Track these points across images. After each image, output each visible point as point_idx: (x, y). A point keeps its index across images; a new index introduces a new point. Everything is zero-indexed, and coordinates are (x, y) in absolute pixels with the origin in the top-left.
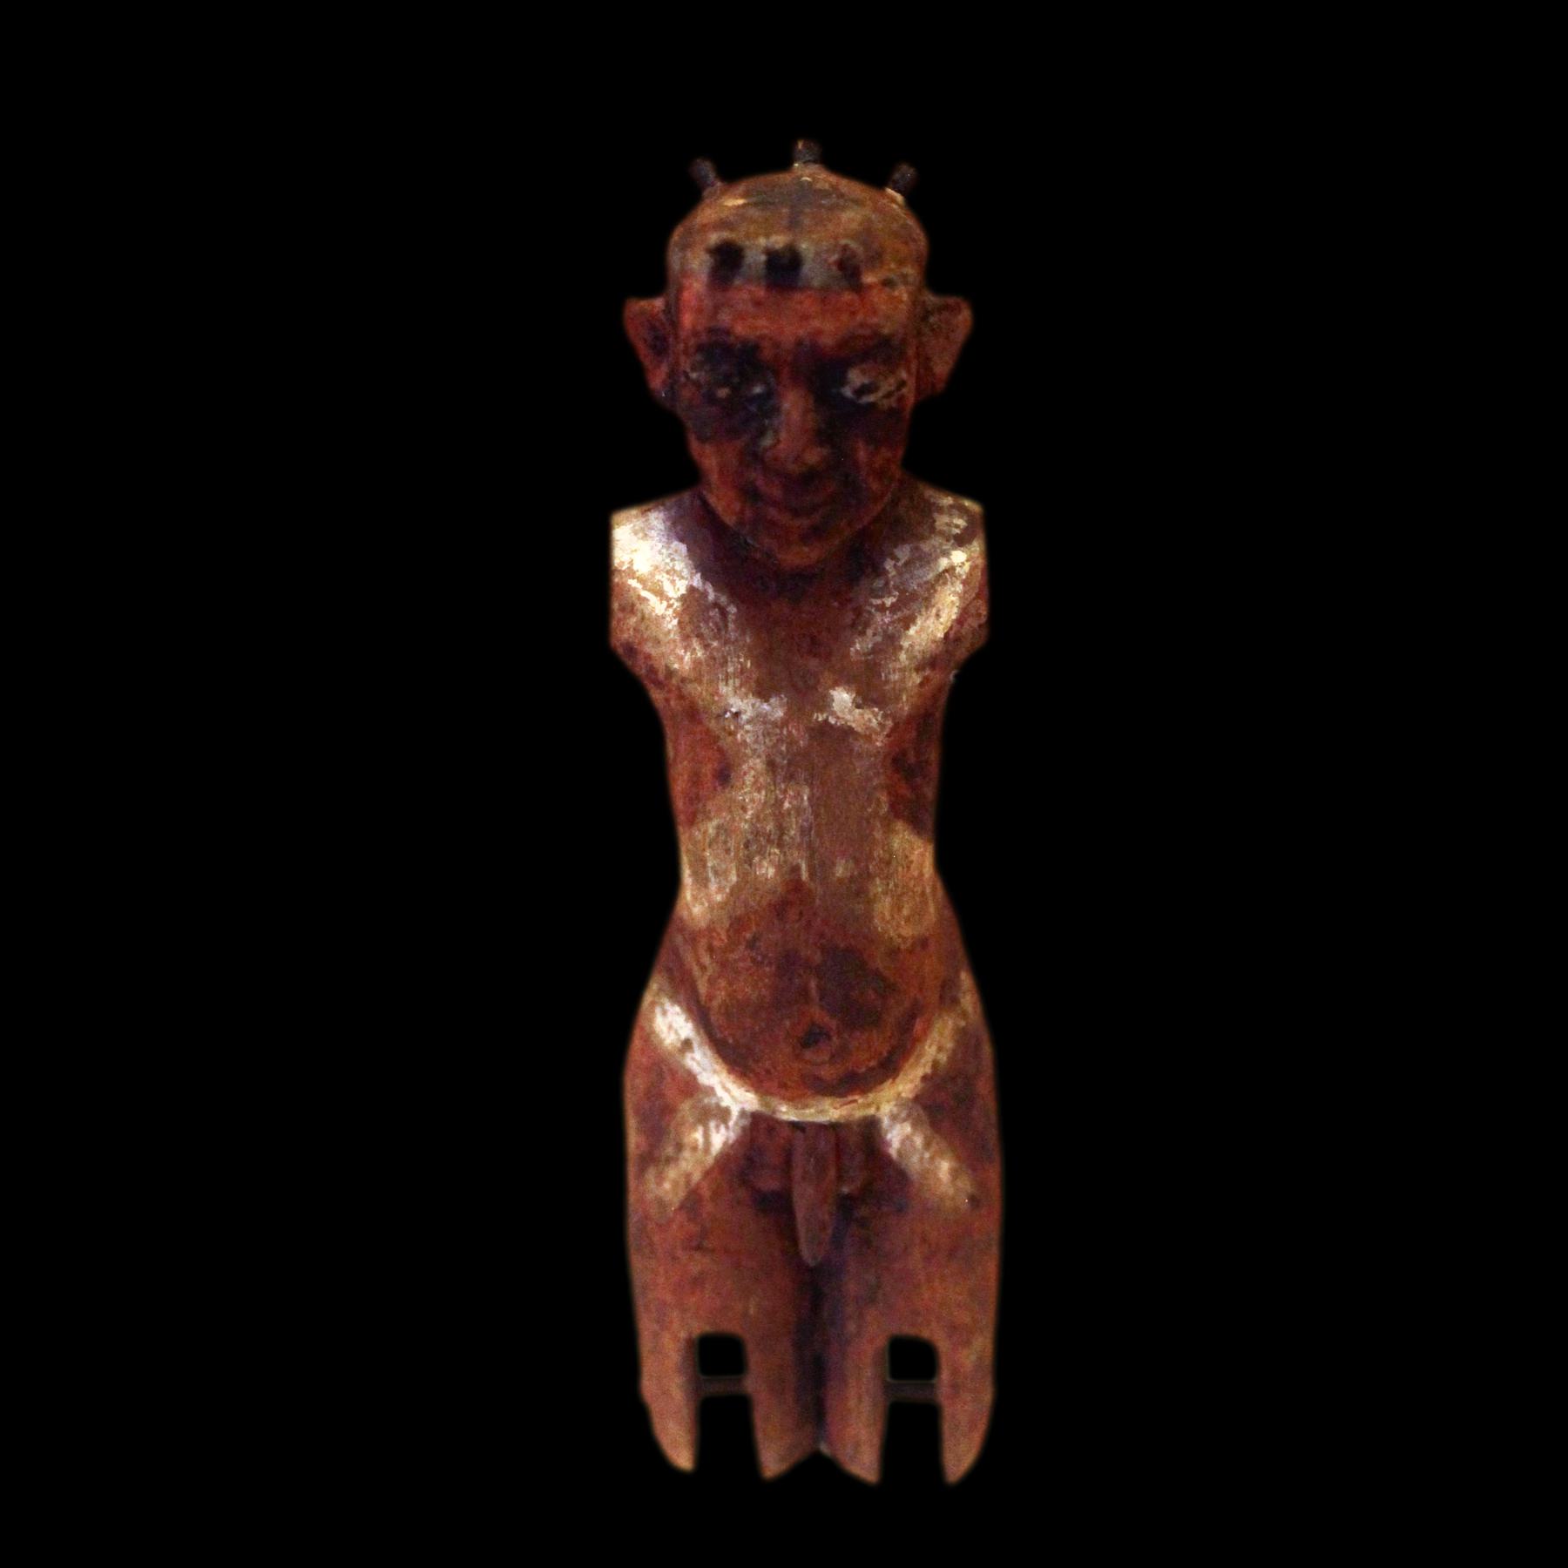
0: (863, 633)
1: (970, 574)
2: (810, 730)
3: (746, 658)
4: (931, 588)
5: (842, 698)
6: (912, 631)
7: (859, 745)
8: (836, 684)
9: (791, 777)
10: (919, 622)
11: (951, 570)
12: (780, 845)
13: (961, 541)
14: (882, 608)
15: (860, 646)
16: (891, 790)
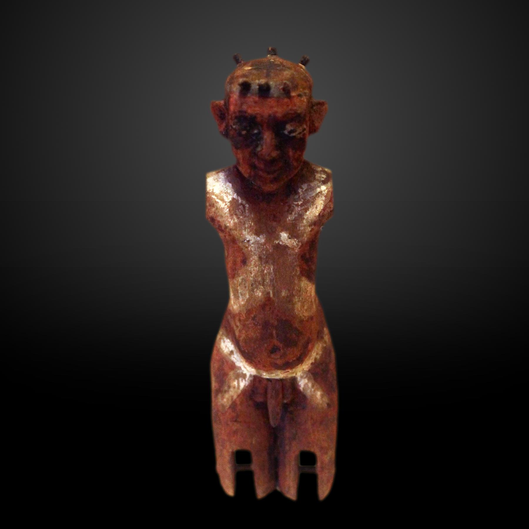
0: (291, 214)
1: (327, 194)
2: (273, 246)
3: (252, 222)
4: (314, 198)
5: (284, 235)
6: (308, 213)
7: (290, 251)
8: (282, 231)
9: (267, 262)
10: (310, 210)
11: (321, 192)
12: (263, 285)
14: (297, 205)
15: (290, 218)
16: (301, 267)
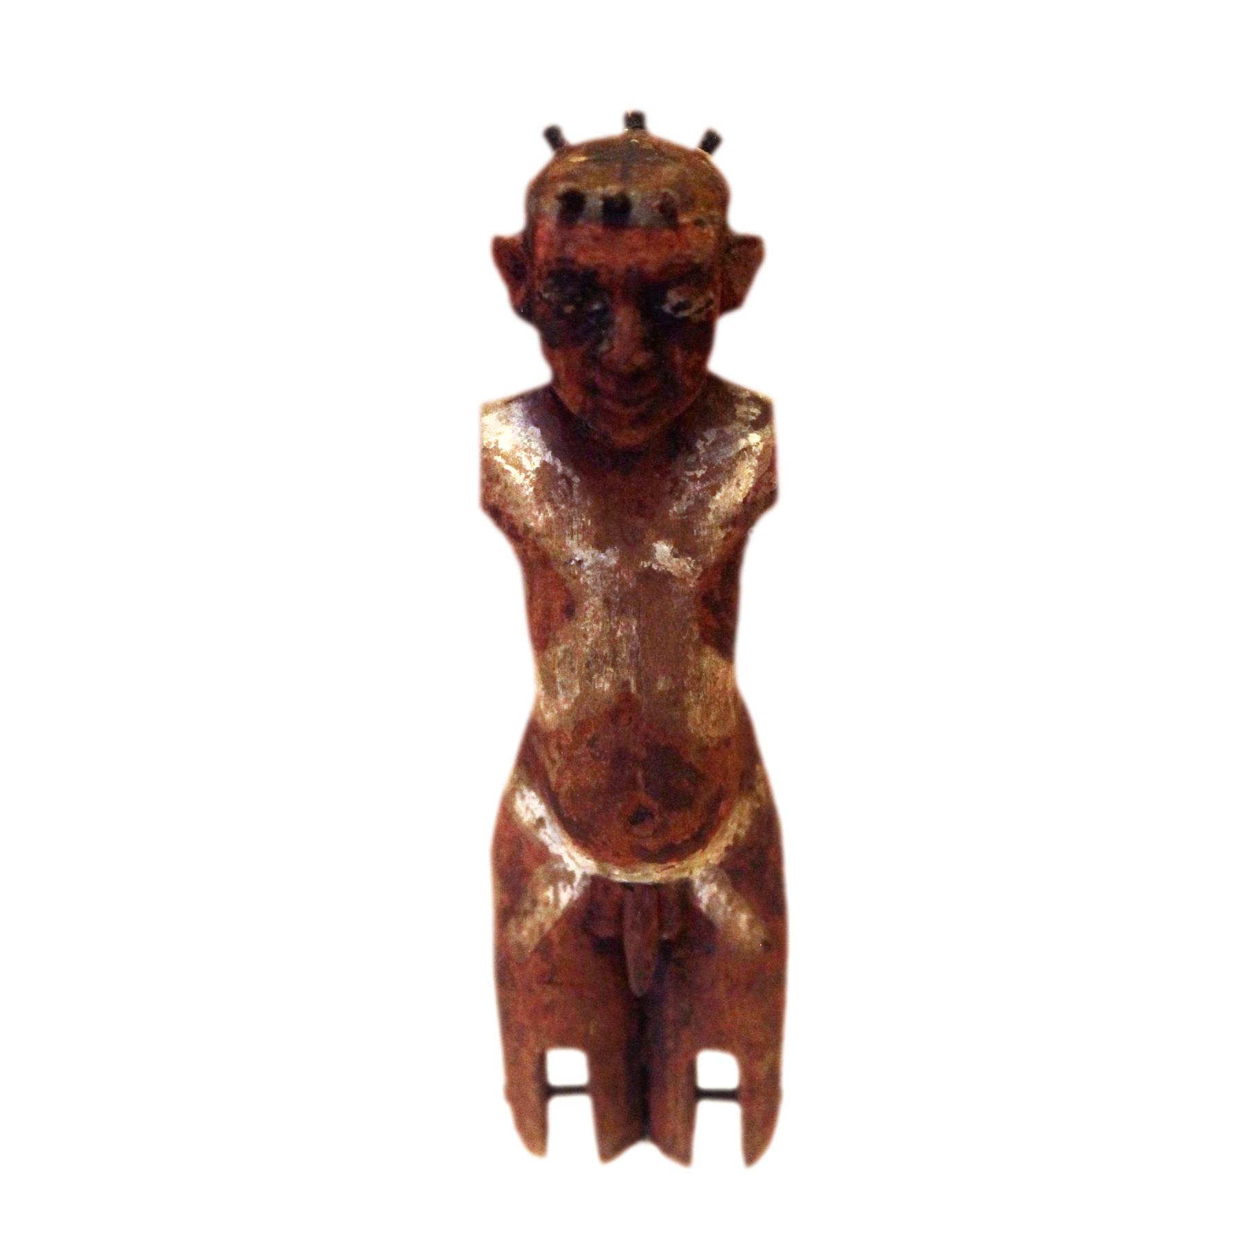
0: (679, 498)
2: (638, 574)
3: (587, 518)
4: (733, 463)
5: (663, 549)
6: (718, 497)
7: (676, 587)
8: (658, 538)
9: (622, 612)
10: (723, 489)
11: (748, 448)
12: (614, 665)
14: (694, 479)
15: (677, 508)
16: (701, 622)
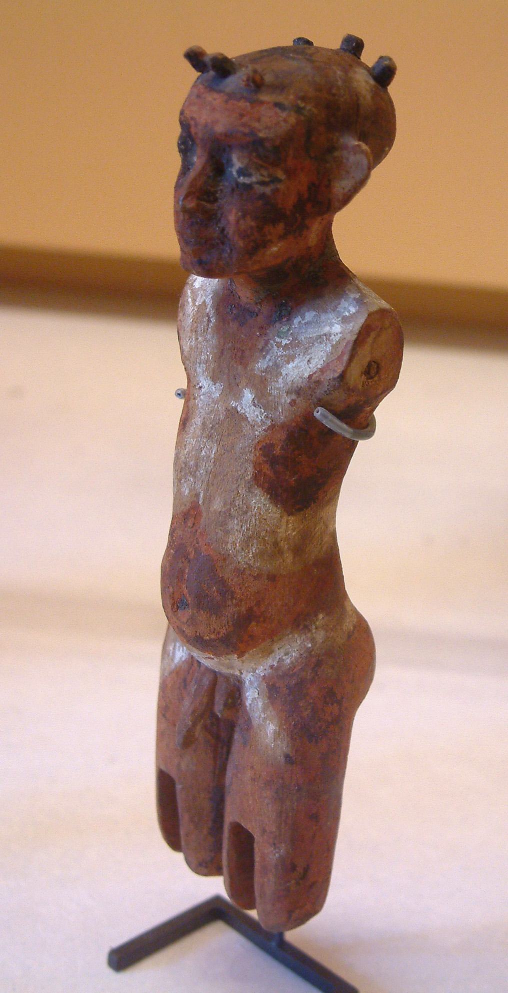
0: (264, 357)
1: (339, 342)
2: (227, 410)
3: (211, 353)
4: (312, 342)
5: (248, 395)
6: (290, 366)
7: (247, 430)
8: (247, 386)
9: (210, 437)
10: (296, 361)
11: (328, 335)
12: (194, 476)
13: (345, 320)
14: (279, 345)
15: (261, 365)
16: (256, 465)
